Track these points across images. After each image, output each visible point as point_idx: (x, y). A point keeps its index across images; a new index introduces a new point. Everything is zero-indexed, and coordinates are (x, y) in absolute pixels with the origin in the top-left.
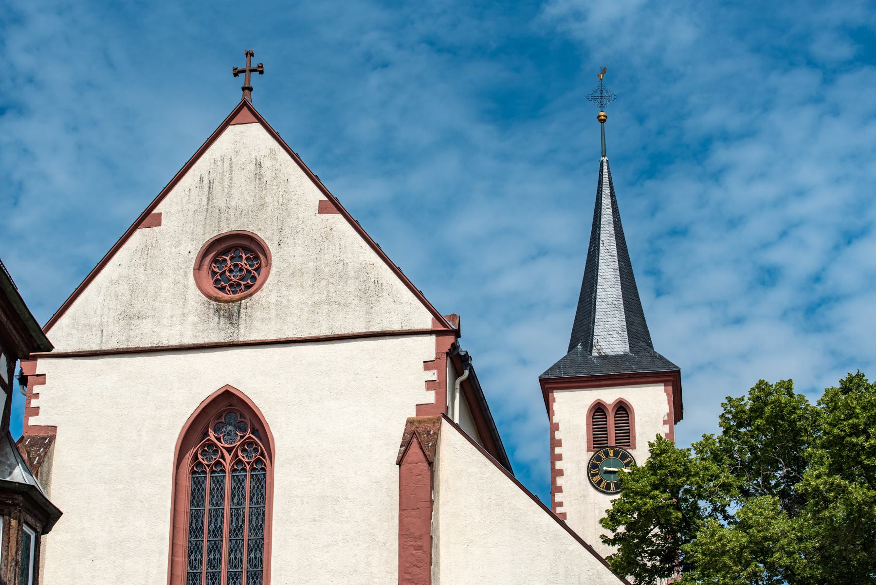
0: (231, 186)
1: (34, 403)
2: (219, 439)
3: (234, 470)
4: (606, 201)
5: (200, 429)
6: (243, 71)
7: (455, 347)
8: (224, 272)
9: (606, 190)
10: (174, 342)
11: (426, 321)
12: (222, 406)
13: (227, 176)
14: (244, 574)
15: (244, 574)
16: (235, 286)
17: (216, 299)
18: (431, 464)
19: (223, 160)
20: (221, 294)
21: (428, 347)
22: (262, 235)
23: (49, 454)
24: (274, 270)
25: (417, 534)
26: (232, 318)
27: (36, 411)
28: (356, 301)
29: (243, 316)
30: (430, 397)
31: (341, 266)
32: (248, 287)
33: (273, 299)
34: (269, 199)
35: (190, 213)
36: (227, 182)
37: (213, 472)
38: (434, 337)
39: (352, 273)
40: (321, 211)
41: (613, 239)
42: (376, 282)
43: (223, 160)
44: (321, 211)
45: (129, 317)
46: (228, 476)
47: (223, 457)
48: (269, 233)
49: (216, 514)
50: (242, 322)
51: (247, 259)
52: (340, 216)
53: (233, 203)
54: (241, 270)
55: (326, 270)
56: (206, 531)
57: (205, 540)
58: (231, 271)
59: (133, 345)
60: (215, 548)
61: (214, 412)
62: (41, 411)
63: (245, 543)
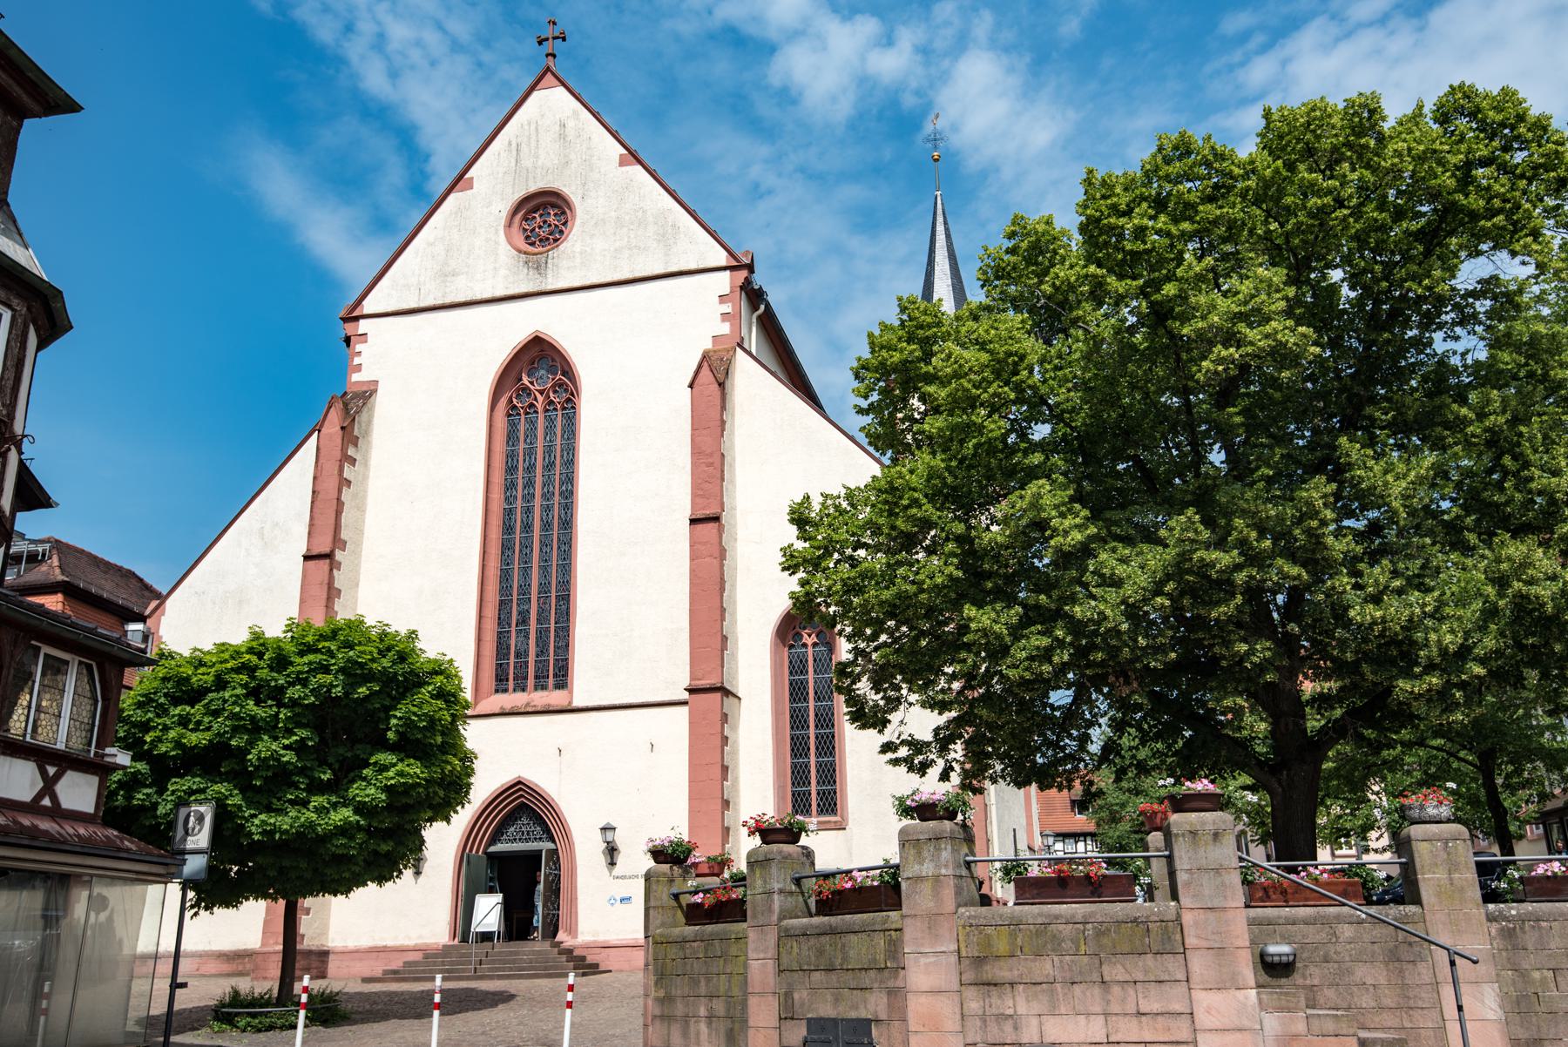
0: (537, 148)
1: (357, 361)
2: (532, 383)
3: (547, 411)
4: (940, 228)
5: (514, 374)
6: (547, 39)
7: (748, 281)
8: (534, 229)
9: (940, 219)
10: (487, 295)
11: (721, 258)
12: (534, 352)
13: (534, 137)
14: (556, 506)
15: (556, 506)
16: (544, 241)
17: (525, 253)
18: (721, 385)
19: (529, 124)
20: (530, 249)
21: (723, 282)
22: (567, 191)
23: (369, 405)
24: (578, 222)
25: (709, 451)
26: (539, 268)
27: (359, 368)
28: (655, 245)
29: (549, 265)
30: (725, 329)
31: (640, 214)
32: (556, 240)
33: (578, 248)
34: (572, 156)
35: (501, 175)
36: (533, 144)
37: (527, 413)
38: (728, 272)
39: (651, 219)
40: (622, 164)
41: (947, 261)
42: (673, 226)
43: (529, 124)
44: (622, 164)
45: (445, 275)
46: (541, 416)
47: (536, 399)
48: (573, 188)
49: (530, 452)
50: (549, 272)
51: (555, 215)
52: (639, 167)
53: (540, 163)
54: (550, 225)
55: (627, 218)
56: (521, 469)
57: (520, 477)
58: (540, 227)
59: (448, 301)
60: (529, 483)
61: (526, 358)
62: (363, 368)
63: (557, 477)
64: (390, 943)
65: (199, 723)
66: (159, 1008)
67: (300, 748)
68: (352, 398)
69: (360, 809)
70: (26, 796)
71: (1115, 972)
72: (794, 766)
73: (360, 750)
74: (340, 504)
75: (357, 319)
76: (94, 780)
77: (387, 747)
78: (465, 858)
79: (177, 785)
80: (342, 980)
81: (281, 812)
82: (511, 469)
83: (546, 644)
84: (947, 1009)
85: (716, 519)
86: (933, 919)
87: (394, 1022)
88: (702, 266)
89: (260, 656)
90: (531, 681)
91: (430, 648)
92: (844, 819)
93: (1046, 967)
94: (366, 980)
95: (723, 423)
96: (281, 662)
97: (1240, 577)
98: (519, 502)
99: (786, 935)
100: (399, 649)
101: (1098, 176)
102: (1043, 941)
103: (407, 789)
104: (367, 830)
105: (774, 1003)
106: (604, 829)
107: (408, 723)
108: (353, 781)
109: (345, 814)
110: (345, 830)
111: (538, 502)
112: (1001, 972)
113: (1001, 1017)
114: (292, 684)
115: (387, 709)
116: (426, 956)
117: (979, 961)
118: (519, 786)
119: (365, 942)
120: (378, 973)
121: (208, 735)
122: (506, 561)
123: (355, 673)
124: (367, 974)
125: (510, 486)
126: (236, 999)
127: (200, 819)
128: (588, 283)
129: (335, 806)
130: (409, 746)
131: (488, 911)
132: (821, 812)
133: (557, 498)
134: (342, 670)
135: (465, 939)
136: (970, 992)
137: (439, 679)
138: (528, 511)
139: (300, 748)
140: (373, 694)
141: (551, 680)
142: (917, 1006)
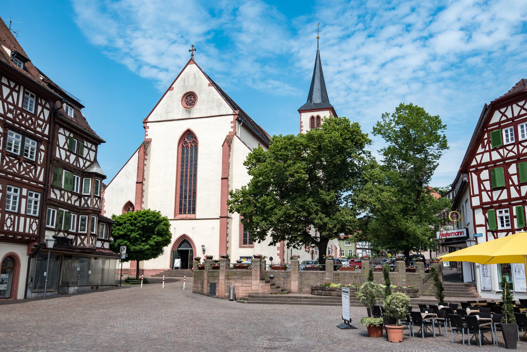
10: (177, 118)
12: (188, 133)
13: (188, 77)
16: (190, 104)
17: (186, 108)
18: (229, 146)
20: (187, 106)
22: (196, 92)
24: (198, 101)
26: (189, 112)
27: (147, 135)
30: (232, 130)
32: (193, 104)
34: (197, 83)
39: (215, 101)
40: (209, 86)
44: (209, 86)
45: (167, 113)
46: (190, 149)
49: (187, 157)
59: (168, 119)
60: (187, 165)
61: (186, 134)
64: (157, 268)
65: (121, 230)
66: (119, 279)
67: (139, 234)
68: (146, 143)
69: (150, 245)
70: (100, 247)
71: (244, 278)
72: (244, 233)
73: (150, 234)
74: (144, 170)
75: (146, 123)
76: (108, 243)
77: (155, 234)
78: (173, 251)
79: (119, 241)
80: (147, 275)
81: (136, 246)
82: (183, 161)
83: (191, 204)
84: (223, 282)
85: (227, 178)
86: (223, 271)
87: (157, 284)
88: (227, 114)
89: (132, 217)
90: (187, 212)
91: (163, 215)
92: (254, 246)
93: (236, 277)
94: (152, 276)
95: (229, 155)
96: (135, 219)
97: (296, 215)
98: (184, 170)
99: (209, 272)
100: (156, 215)
101: (283, 136)
102: (235, 274)
103: (159, 242)
104: (152, 249)
105: (207, 281)
106: (202, 246)
107: (158, 230)
108: (149, 240)
109: (147, 247)
110: (148, 249)
111: (189, 170)
112: (230, 277)
113: (230, 283)
114: (138, 223)
115: (155, 227)
116: (165, 272)
117: (228, 276)
118: (184, 236)
119: (152, 268)
120: (154, 275)
121: (123, 232)
122: (182, 184)
123: (149, 221)
124: (152, 275)
125: (182, 166)
126: (129, 279)
127: (124, 248)
128: (200, 117)
129: (146, 245)
130: (159, 234)
131: (178, 263)
132: (249, 244)
133: (193, 169)
134: (147, 220)
135: (173, 268)
136: (226, 280)
137: (164, 221)
138: (187, 172)
139: (139, 234)
140: (152, 225)
141: (192, 212)
142: (220, 281)
